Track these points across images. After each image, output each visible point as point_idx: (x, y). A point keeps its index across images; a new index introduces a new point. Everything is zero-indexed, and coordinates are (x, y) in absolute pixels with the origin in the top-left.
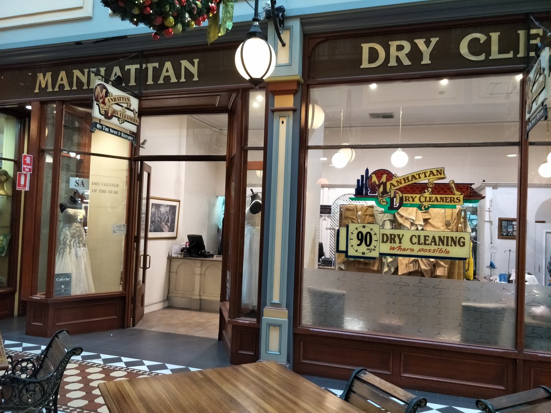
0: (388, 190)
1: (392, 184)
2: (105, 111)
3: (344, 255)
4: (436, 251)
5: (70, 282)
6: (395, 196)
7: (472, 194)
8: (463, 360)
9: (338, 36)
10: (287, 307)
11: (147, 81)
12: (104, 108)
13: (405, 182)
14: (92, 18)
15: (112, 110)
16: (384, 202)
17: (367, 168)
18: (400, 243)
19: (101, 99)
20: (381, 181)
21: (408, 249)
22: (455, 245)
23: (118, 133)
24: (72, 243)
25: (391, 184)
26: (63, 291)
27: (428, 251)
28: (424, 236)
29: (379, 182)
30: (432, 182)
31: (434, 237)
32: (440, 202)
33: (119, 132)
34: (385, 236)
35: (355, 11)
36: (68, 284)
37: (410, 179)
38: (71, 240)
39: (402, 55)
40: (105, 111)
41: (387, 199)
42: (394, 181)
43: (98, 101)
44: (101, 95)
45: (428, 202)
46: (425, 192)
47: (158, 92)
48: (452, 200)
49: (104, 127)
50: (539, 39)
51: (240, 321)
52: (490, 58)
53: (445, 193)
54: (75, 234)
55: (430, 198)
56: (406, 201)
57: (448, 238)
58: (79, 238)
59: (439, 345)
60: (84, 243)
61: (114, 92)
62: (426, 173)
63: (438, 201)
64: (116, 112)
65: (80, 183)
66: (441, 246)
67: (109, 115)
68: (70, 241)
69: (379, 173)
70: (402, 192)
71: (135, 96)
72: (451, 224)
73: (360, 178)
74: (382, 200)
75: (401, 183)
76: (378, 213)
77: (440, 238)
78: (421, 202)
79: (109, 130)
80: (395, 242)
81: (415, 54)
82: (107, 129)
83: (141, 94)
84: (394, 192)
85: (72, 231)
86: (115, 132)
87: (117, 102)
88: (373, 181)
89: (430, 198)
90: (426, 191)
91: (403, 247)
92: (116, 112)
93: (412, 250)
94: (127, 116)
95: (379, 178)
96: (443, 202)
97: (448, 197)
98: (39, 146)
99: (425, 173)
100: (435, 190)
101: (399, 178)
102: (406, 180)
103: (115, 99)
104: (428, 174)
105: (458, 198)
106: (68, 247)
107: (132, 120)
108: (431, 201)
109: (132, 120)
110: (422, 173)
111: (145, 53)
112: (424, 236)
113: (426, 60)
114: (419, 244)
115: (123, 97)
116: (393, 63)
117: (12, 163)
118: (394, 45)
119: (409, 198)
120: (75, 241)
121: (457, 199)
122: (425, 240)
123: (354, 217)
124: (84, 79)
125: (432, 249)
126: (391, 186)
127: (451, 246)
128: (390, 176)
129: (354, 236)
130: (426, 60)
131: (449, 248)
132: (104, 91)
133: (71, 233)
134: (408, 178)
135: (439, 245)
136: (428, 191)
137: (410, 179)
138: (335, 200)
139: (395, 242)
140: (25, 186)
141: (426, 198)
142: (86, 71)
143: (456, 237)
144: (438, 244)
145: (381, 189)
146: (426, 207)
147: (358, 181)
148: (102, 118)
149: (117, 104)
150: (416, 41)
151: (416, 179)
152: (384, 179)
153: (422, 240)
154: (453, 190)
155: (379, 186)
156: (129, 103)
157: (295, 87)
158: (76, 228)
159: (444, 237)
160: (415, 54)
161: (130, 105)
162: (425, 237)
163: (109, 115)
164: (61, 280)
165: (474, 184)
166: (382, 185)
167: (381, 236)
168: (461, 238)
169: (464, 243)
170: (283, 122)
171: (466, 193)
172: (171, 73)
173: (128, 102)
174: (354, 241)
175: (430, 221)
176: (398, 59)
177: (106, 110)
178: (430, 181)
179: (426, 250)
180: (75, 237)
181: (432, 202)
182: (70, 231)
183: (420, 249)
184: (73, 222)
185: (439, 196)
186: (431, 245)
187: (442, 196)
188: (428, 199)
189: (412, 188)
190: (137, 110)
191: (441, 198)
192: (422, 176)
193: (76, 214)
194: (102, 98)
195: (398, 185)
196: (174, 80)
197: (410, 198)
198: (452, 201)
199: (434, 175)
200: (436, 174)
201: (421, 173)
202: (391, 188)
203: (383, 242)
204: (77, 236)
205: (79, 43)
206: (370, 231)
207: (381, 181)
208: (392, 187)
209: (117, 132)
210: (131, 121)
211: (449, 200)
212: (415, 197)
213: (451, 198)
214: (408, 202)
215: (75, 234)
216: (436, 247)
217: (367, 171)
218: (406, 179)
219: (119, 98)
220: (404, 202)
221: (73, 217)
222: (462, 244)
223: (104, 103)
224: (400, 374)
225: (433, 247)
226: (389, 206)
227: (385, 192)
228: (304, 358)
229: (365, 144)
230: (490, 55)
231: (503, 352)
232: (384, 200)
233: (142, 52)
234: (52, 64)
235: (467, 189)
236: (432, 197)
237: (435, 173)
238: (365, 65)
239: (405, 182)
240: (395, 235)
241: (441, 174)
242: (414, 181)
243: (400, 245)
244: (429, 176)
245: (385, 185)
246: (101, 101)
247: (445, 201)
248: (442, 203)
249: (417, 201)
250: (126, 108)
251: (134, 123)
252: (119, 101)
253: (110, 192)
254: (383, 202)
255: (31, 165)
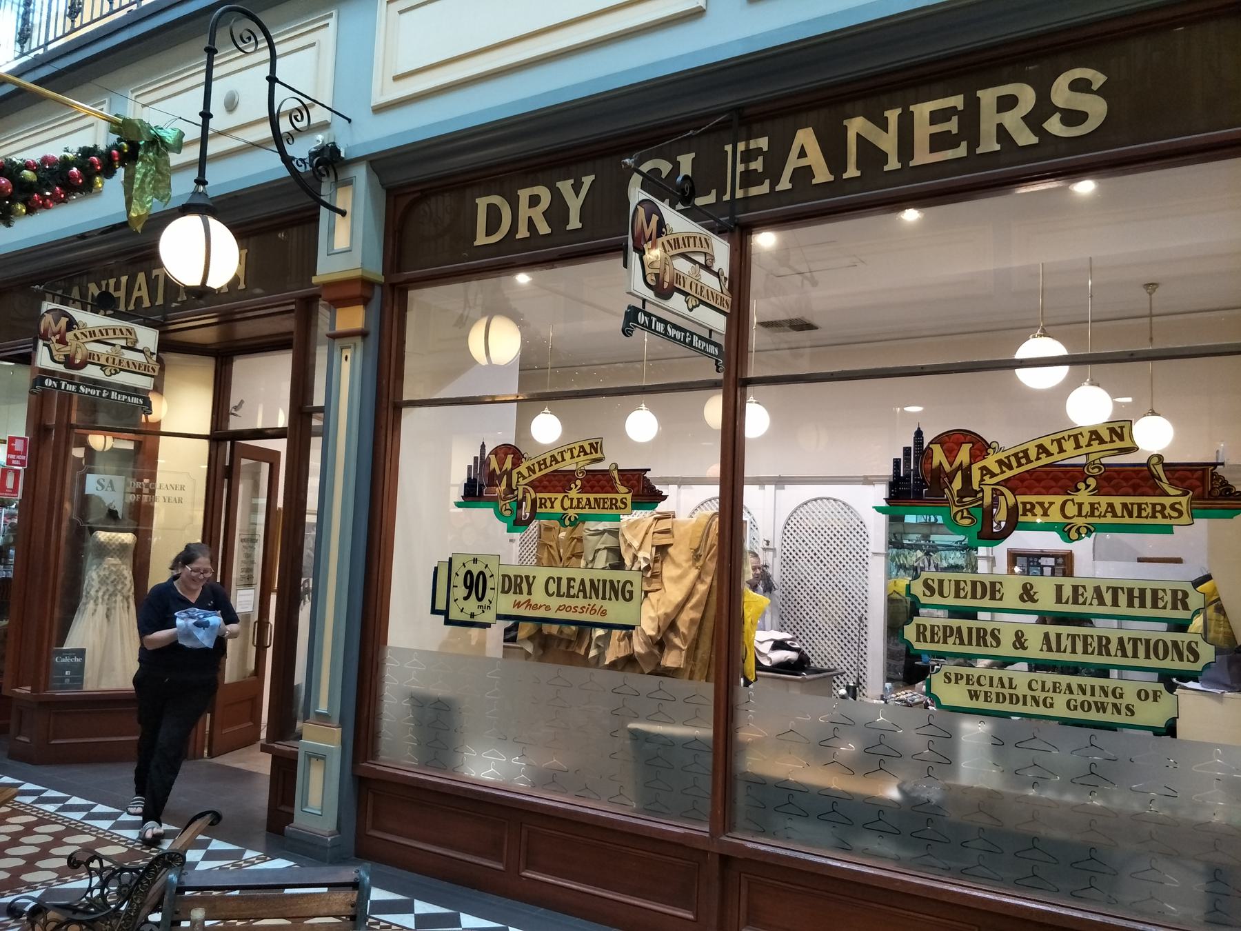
0: (976, 486)
1: (985, 471)
2: (657, 275)
3: (442, 618)
4: (585, 610)
5: (82, 665)
6: (524, 498)
7: (646, 491)
8: (624, 848)
9: (1182, 16)
10: (342, 723)
11: (567, 222)
12: (61, 351)
13: (1020, 465)
14: (704, 11)
15: (85, 352)
16: (965, 518)
17: (919, 428)
18: (529, 593)
19: (54, 335)
20: (504, 469)
21: (541, 606)
22: (617, 599)
23: (685, 337)
24: (100, 594)
25: (983, 468)
26: (67, 681)
27: (573, 610)
28: (567, 578)
29: (501, 470)
30: (1098, 462)
31: (582, 582)
32: (1123, 516)
33: (688, 334)
34: (507, 579)
35: (675, 77)
36: (79, 670)
37: (1033, 454)
38: (100, 588)
39: (1012, 120)
40: (657, 275)
41: (509, 504)
42: (990, 462)
43: (49, 340)
44: (55, 329)
45: (1086, 516)
46: (571, 489)
47: (287, 295)
48: (614, 505)
49: (654, 319)
50: (955, 119)
51: (276, 746)
52: (979, 151)
53: (1136, 491)
54: (107, 578)
55: (1092, 505)
56: (541, 507)
57: (604, 582)
58: (115, 586)
59: (576, 813)
60: (125, 594)
61: (677, 222)
62: (1063, 441)
63: (1115, 515)
64: (682, 280)
65: (106, 484)
66: (594, 601)
67: (666, 285)
68: (97, 591)
69: (951, 440)
70: (1014, 491)
71: (720, 231)
72: (700, 556)
73: (900, 455)
74: (504, 507)
75: (1010, 468)
76: (590, 535)
77: (592, 581)
78: (1065, 517)
79: (666, 329)
80: (521, 593)
81: (557, 212)
82: (660, 327)
83: (166, 319)
84: (993, 489)
85: (102, 573)
86: (679, 335)
87: (99, 337)
88: (935, 463)
89: (1092, 505)
90: (1081, 486)
91: (533, 603)
92: (682, 280)
93: (548, 608)
94: (126, 361)
95: (951, 453)
96: (1131, 515)
97: (1146, 504)
98: (40, 420)
99: (1076, 437)
100: (586, 484)
101: (1006, 454)
102: (1022, 458)
103: (676, 241)
104: (576, 453)
105: (1177, 506)
106: (92, 602)
107: (717, 299)
108: (1097, 513)
109: (717, 299)
110: (1069, 437)
111: (747, 112)
112: (567, 578)
113: (574, 223)
114: (559, 595)
115: (694, 235)
116: (523, 233)
117: (206, 443)
118: (524, 194)
119: (1033, 506)
120: (108, 590)
121: (1173, 507)
122: (569, 587)
123: (553, 544)
124: (888, 142)
125: (580, 607)
126: (983, 475)
127: (610, 599)
128: (981, 447)
129: (458, 581)
130: (574, 223)
131: (607, 605)
132: (655, 218)
133: (99, 576)
134: (1025, 452)
135: (591, 598)
136: (1088, 486)
137: (1033, 455)
138: (691, 510)
139: (521, 593)
140: (15, 490)
141: (1080, 505)
142: (893, 115)
143: (618, 582)
144: (588, 595)
145: (957, 484)
146: (573, 519)
147: (897, 463)
148: (649, 294)
149: (684, 255)
150: (559, 184)
151: (557, 462)
152: (964, 455)
153: (564, 589)
154: (616, 483)
155: (951, 477)
156: (133, 337)
157: (357, 290)
158: (109, 567)
159: (599, 581)
160: (557, 212)
161: (136, 341)
162: (569, 580)
163: (666, 285)
164: (66, 660)
165: (649, 470)
166: (959, 473)
167: (501, 578)
168: (626, 582)
169: (631, 593)
170: (346, 358)
171: (636, 489)
172: (816, 159)
173: (129, 336)
174: (460, 592)
175: (670, 550)
176: (1002, 133)
177: (657, 272)
178: (1092, 457)
179: (569, 609)
180: (107, 584)
181: (1099, 516)
182: (98, 573)
183: (560, 606)
184: (105, 556)
185: (1117, 501)
186: (578, 597)
187: (1129, 500)
188: (1086, 509)
189: (550, 481)
190: (726, 274)
191: (1124, 505)
192: (567, 456)
193: (111, 540)
194: (59, 332)
195: (1003, 472)
196: (822, 175)
197: (1037, 507)
198: (1158, 515)
199: (1102, 442)
200: (1107, 438)
201: (1064, 438)
202: (982, 480)
203: (503, 592)
204: (112, 582)
205: (82, 236)
206: (483, 569)
207: (504, 469)
208: (987, 478)
209: (683, 334)
210: (714, 304)
211: (1149, 510)
212: (1051, 504)
213: (1154, 505)
214: (543, 510)
215: (107, 578)
216: (585, 602)
217: (919, 434)
218: (1021, 455)
219: (688, 239)
220: (1021, 519)
221: (105, 546)
222: (627, 596)
223: (62, 341)
224: (519, 872)
225: (580, 602)
226: (978, 527)
227: (510, 490)
228: (375, 828)
229: (980, 360)
230: (912, 158)
231: (685, 835)
232: (508, 507)
233: (738, 110)
234: (525, 168)
235: (1202, 480)
236: (1099, 503)
237: (1106, 435)
238: (482, 239)
239: (1020, 465)
240: (521, 577)
241: (1121, 438)
242: (555, 467)
243: (529, 597)
244: (1089, 445)
245: (509, 474)
246: (54, 339)
247: (1135, 514)
248: (597, 511)
249: (1055, 516)
250: (123, 347)
251: (721, 308)
252: (685, 247)
253: (167, 500)
254: (506, 510)
255: (24, 454)
